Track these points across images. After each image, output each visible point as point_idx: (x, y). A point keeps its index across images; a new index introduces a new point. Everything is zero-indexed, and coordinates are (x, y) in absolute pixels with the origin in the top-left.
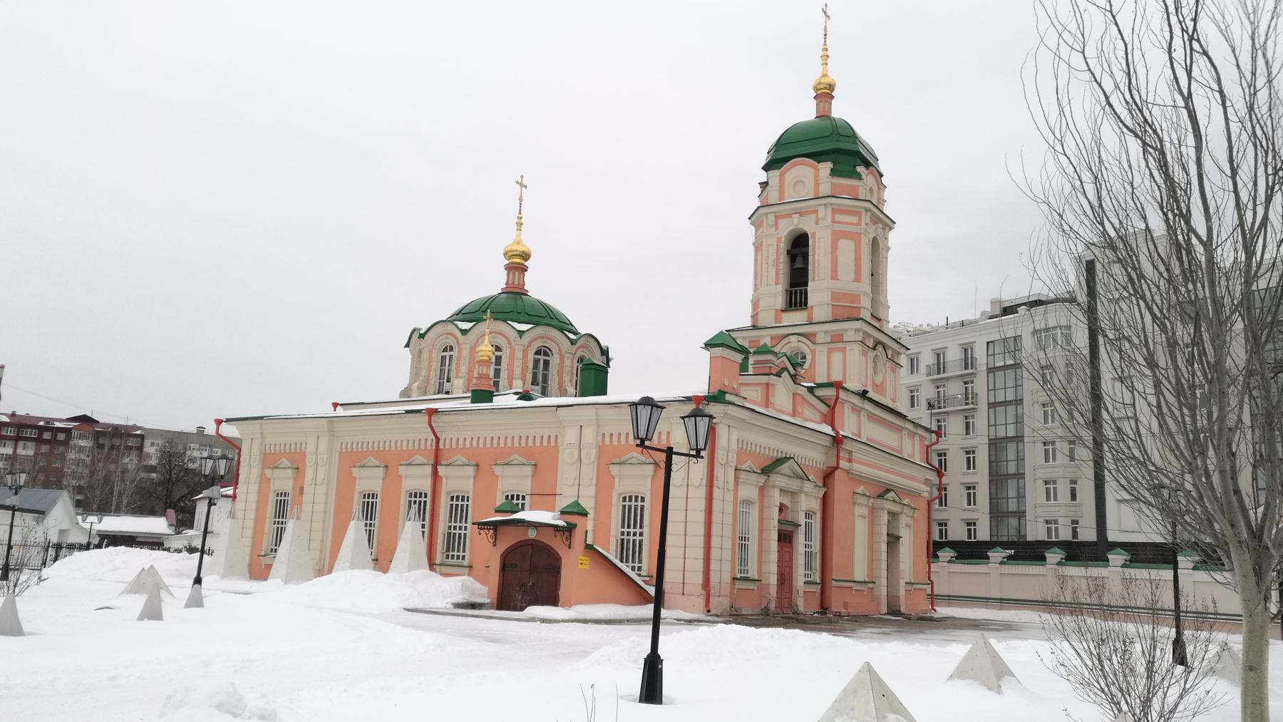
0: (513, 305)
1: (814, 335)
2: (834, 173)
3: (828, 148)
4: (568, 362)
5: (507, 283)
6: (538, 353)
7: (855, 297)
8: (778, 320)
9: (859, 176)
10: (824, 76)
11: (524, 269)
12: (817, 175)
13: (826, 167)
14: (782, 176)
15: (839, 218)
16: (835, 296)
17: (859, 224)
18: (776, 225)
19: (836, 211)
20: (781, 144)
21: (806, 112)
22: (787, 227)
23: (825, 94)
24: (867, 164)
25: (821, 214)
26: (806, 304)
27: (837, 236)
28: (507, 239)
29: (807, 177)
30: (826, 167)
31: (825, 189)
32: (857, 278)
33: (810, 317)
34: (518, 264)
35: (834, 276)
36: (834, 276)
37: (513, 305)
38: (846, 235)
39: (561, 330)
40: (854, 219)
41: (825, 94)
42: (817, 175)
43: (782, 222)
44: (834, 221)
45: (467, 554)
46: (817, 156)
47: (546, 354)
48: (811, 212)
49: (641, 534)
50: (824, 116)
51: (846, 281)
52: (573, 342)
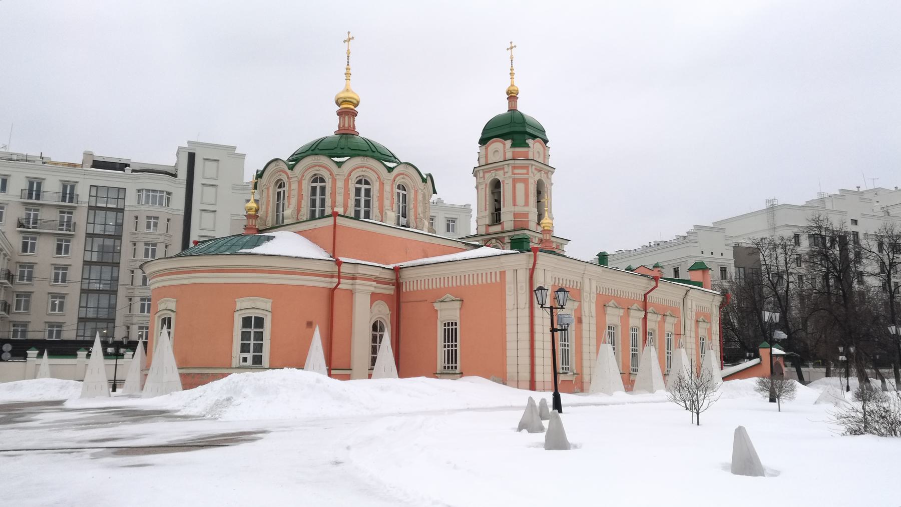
0: (345, 145)
1: (504, 237)
2: (513, 146)
3: (512, 131)
4: (387, 188)
5: (339, 126)
6: (359, 182)
7: (526, 215)
8: (487, 229)
9: (527, 146)
10: (512, 85)
11: (355, 114)
12: (504, 147)
13: (509, 143)
14: (486, 148)
15: (516, 171)
16: (516, 215)
17: (527, 174)
18: (484, 177)
19: (514, 168)
20: (485, 130)
21: (502, 108)
22: (489, 178)
23: (512, 96)
24: (534, 137)
25: (506, 170)
26: (500, 220)
27: (515, 181)
28: (337, 88)
29: (501, 148)
30: (509, 143)
31: (509, 155)
32: (527, 204)
33: (503, 228)
34: (347, 110)
35: (515, 205)
36: (515, 205)
37: (345, 145)
38: (521, 180)
39: (379, 159)
40: (524, 171)
41: (512, 96)
42: (504, 147)
43: (487, 175)
44: (513, 173)
45: (458, 365)
46: (504, 136)
47: (367, 183)
48: (500, 169)
49: (456, 346)
50: (513, 110)
51: (520, 209)
52: (390, 170)
